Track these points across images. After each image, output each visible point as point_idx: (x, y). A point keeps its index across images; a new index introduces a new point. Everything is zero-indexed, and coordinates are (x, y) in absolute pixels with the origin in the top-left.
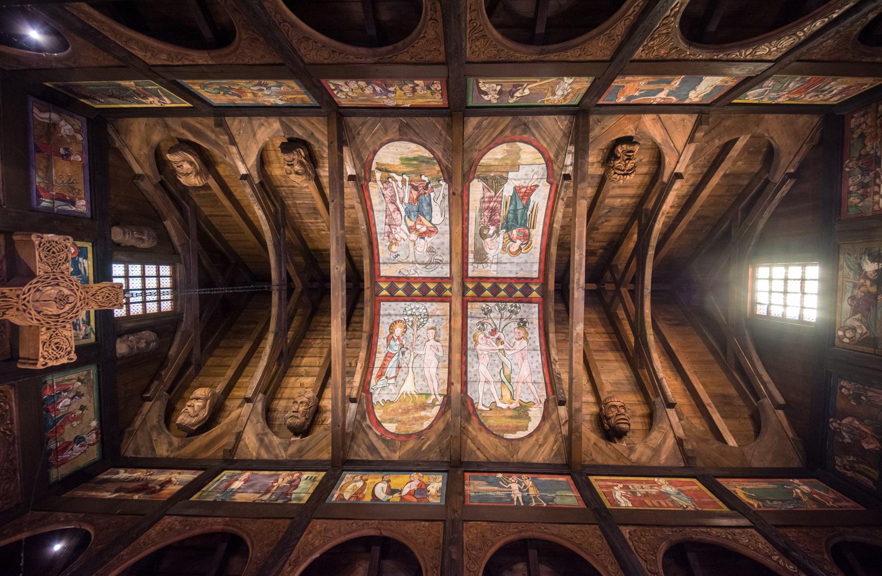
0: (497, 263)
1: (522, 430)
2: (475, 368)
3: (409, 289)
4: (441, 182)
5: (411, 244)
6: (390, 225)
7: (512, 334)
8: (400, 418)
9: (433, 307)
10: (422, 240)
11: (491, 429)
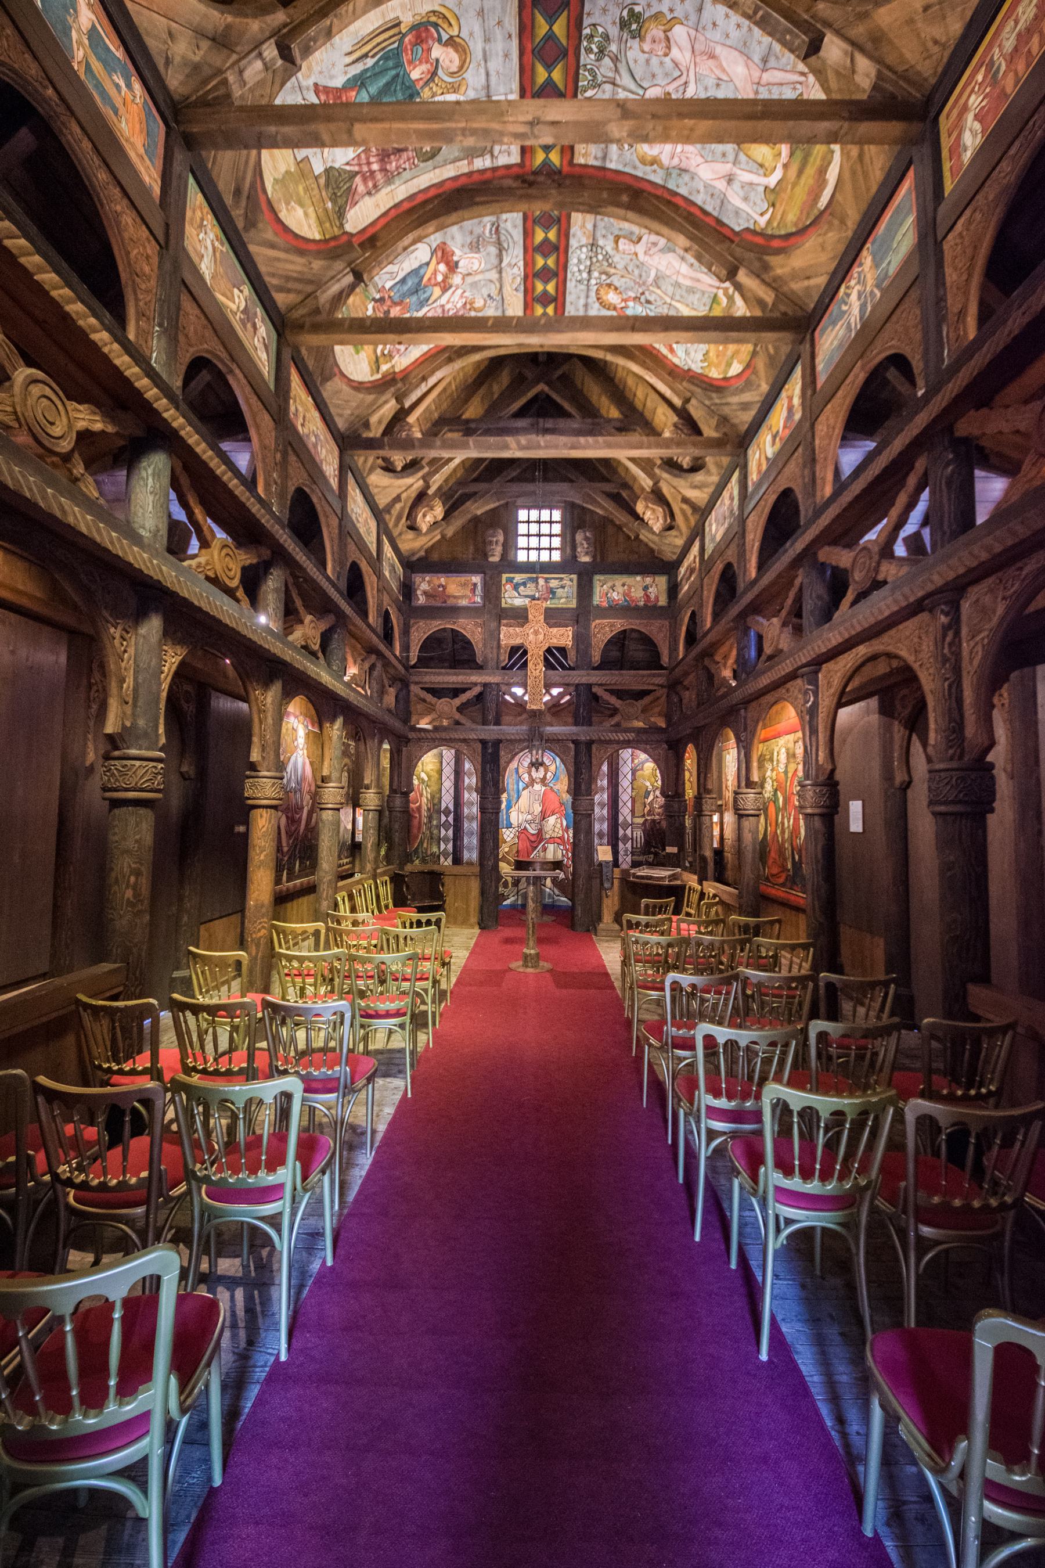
1: (829, 163)
2: (702, 189)
3: (545, 274)
5: (469, 280)
7: (655, 61)
9: (579, 233)
10: (461, 264)
11: (801, 226)
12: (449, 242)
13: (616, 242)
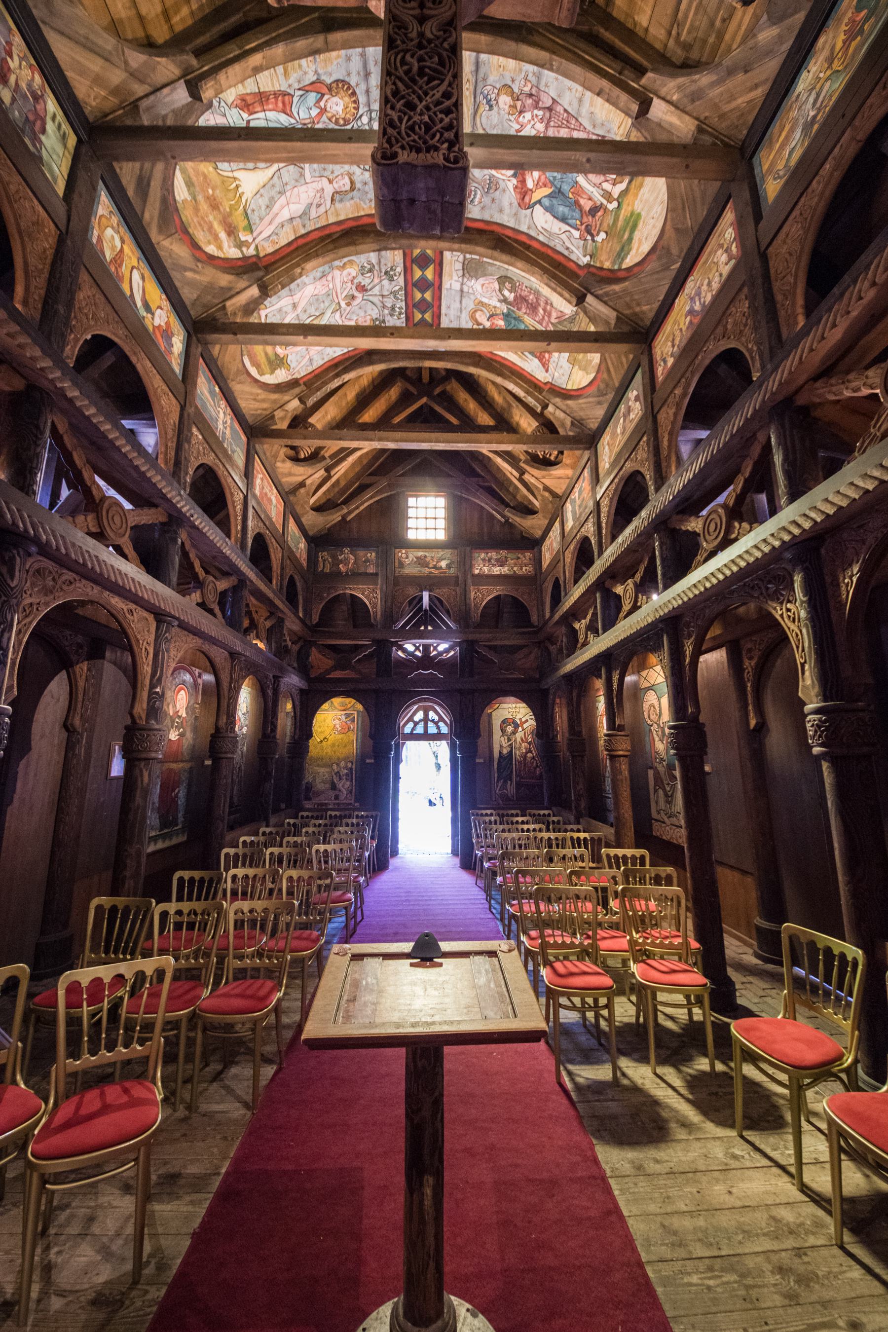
0: (462, 291)
4: (588, 258)
6: (550, 109)
7: (362, 314)
8: (200, 198)
12: (516, 204)
13: (352, 183)
